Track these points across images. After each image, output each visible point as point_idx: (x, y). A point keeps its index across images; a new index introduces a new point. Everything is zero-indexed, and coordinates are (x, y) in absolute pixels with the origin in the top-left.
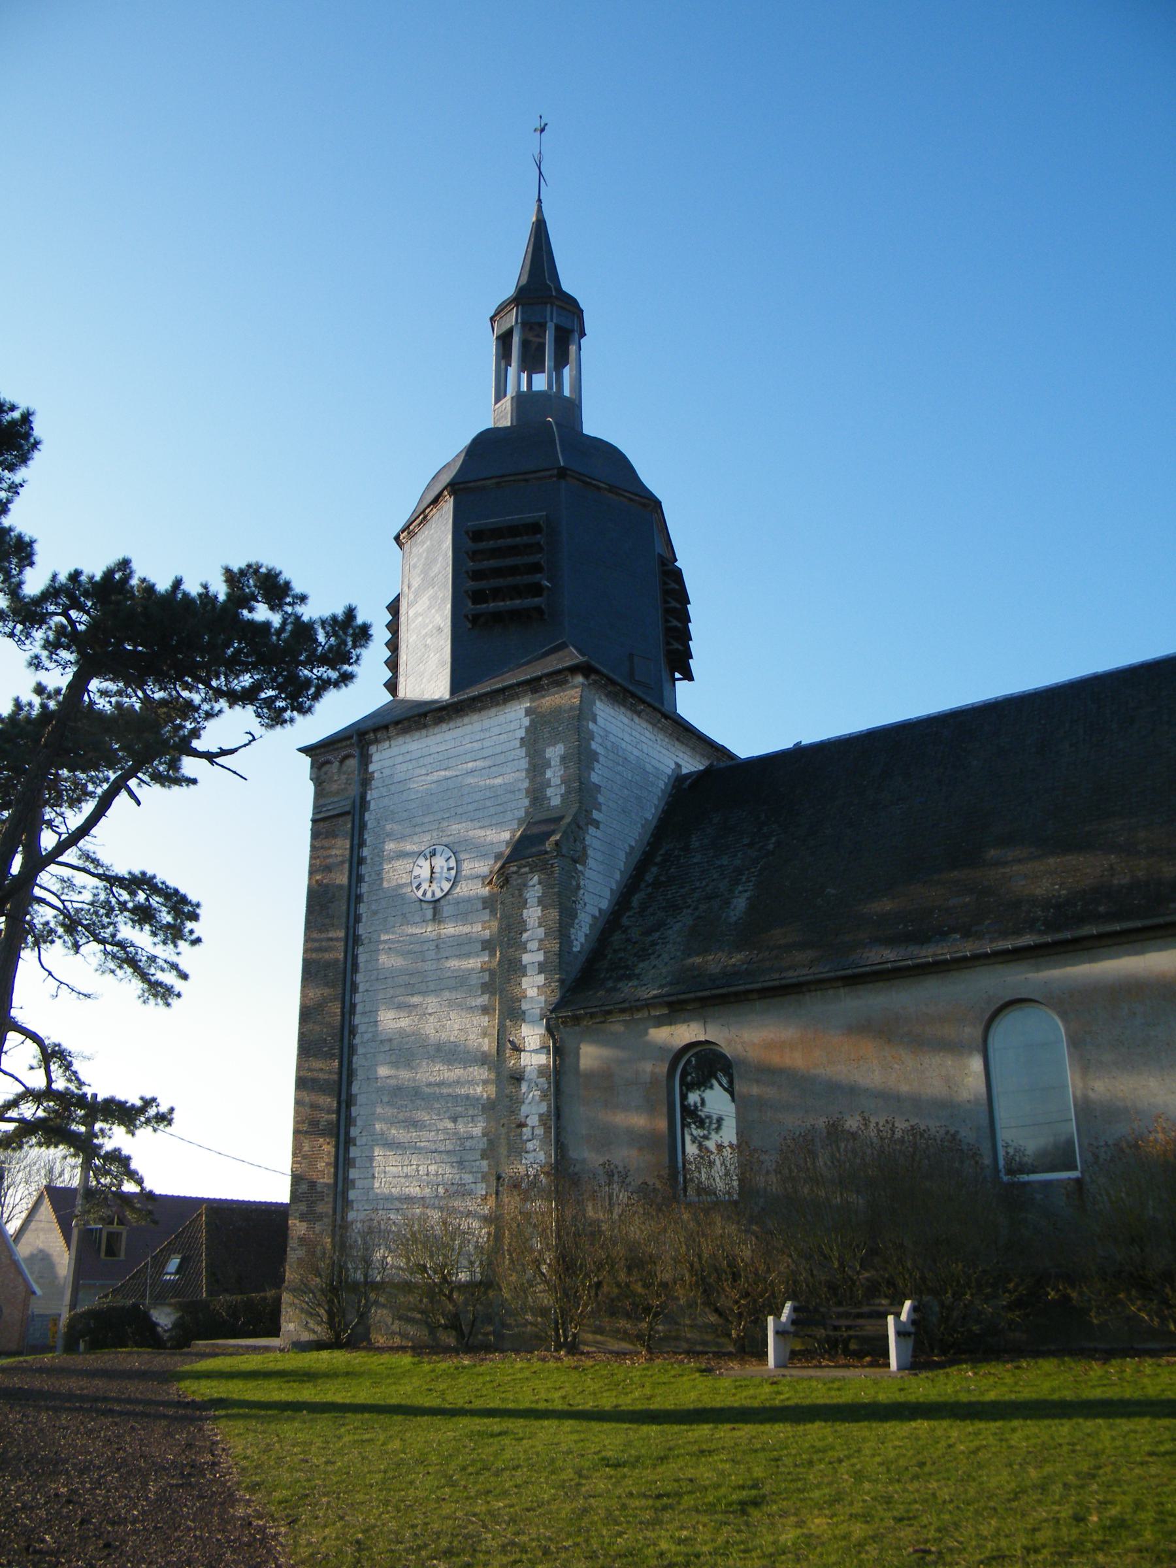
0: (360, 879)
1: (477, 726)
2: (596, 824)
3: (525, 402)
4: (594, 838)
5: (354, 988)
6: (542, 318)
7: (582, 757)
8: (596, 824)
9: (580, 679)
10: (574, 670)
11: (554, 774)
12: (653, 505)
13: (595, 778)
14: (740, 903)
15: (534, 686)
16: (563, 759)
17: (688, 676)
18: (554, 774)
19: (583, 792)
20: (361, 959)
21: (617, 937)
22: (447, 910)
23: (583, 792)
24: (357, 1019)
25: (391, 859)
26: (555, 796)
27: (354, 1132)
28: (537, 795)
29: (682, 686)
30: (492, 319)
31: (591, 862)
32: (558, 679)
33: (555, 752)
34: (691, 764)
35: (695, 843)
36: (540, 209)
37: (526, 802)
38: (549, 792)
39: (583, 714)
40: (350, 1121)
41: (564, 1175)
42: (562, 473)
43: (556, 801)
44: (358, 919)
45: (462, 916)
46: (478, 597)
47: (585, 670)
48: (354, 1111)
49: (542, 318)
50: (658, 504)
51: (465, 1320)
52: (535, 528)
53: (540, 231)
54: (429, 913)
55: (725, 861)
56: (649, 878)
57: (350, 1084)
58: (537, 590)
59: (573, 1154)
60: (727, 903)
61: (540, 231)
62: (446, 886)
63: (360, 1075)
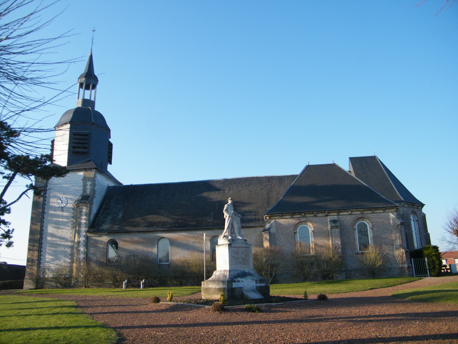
0: (45, 201)
1: (73, 175)
2: (95, 197)
3: (85, 101)
4: (95, 200)
5: (43, 222)
6: (90, 80)
7: (94, 185)
8: (95, 197)
9: (94, 170)
10: (94, 168)
11: (88, 187)
12: (108, 130)
13: (96, 189)
14: (120, 215)
15: (85, 170)
16: (91, 185)
17: (111, 164)
18: (88, 187)
19: (93, 191)
20: (45, 216)
21: (98, 218)
22: (64, 209)
23: (93, 191)
24: (44, 228)
25: (52, 197)
26: (88, 192)
27: (42, 249)
28: (84, 190)
29: (109, 166)
30: (79, 78)
31: (94, 204)
32: (90, 169)
33: (89, 183)
34: (112, 184)
35: (112, 202)
36: (91, 53)
37: (82, 191)
38: (87, 191)
39: (95, 177)
40: (41, 247)
41: (87, 259)
42: (93, 124)
43: (88, 192)
44: (45, 208)
45: (68, 211)
46: (74, 148)
47: (96, 168)
48: (42, 246)
49: (90, 80)
50: (110, 130)
51: (65, 282)
52: (86, 135)
53: (91, 57)
54: (61, 209)
55: (117, 206)
56: (103, 207)
57: (42, 240)
58: (85, 148)
59: (89, 256)
60: (118, 215)
61: (91, 57)
62: (65, 205)
63: (44, 239)
